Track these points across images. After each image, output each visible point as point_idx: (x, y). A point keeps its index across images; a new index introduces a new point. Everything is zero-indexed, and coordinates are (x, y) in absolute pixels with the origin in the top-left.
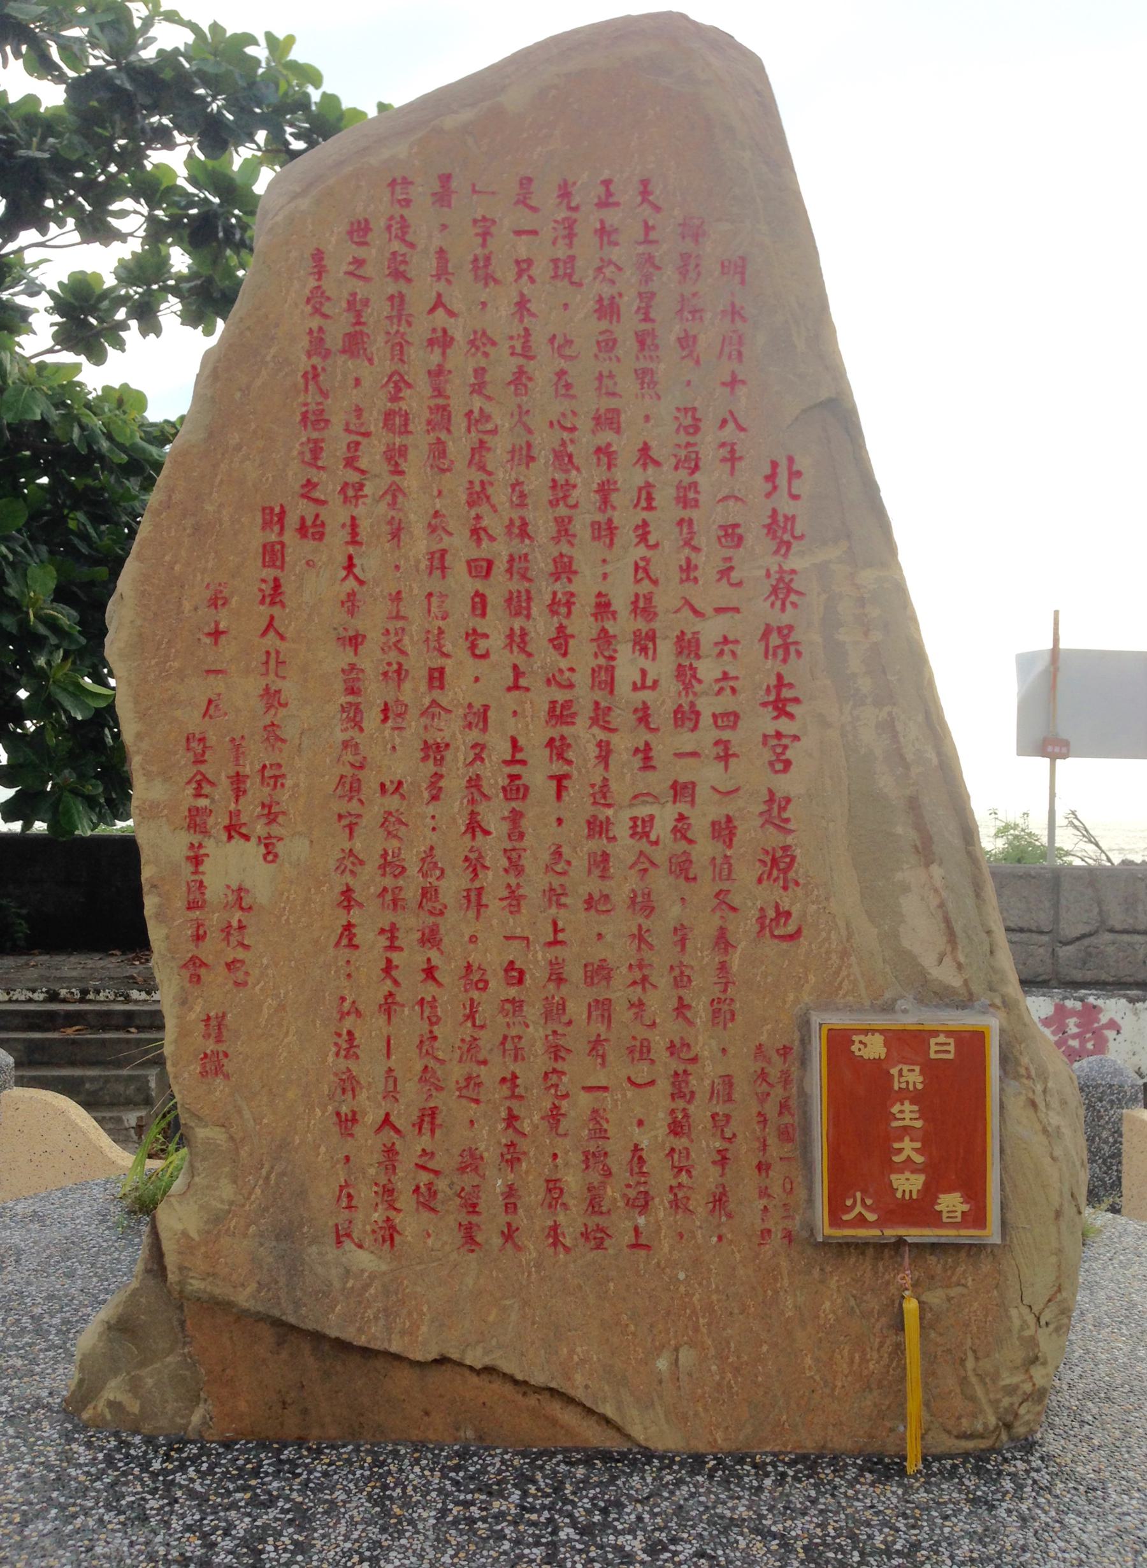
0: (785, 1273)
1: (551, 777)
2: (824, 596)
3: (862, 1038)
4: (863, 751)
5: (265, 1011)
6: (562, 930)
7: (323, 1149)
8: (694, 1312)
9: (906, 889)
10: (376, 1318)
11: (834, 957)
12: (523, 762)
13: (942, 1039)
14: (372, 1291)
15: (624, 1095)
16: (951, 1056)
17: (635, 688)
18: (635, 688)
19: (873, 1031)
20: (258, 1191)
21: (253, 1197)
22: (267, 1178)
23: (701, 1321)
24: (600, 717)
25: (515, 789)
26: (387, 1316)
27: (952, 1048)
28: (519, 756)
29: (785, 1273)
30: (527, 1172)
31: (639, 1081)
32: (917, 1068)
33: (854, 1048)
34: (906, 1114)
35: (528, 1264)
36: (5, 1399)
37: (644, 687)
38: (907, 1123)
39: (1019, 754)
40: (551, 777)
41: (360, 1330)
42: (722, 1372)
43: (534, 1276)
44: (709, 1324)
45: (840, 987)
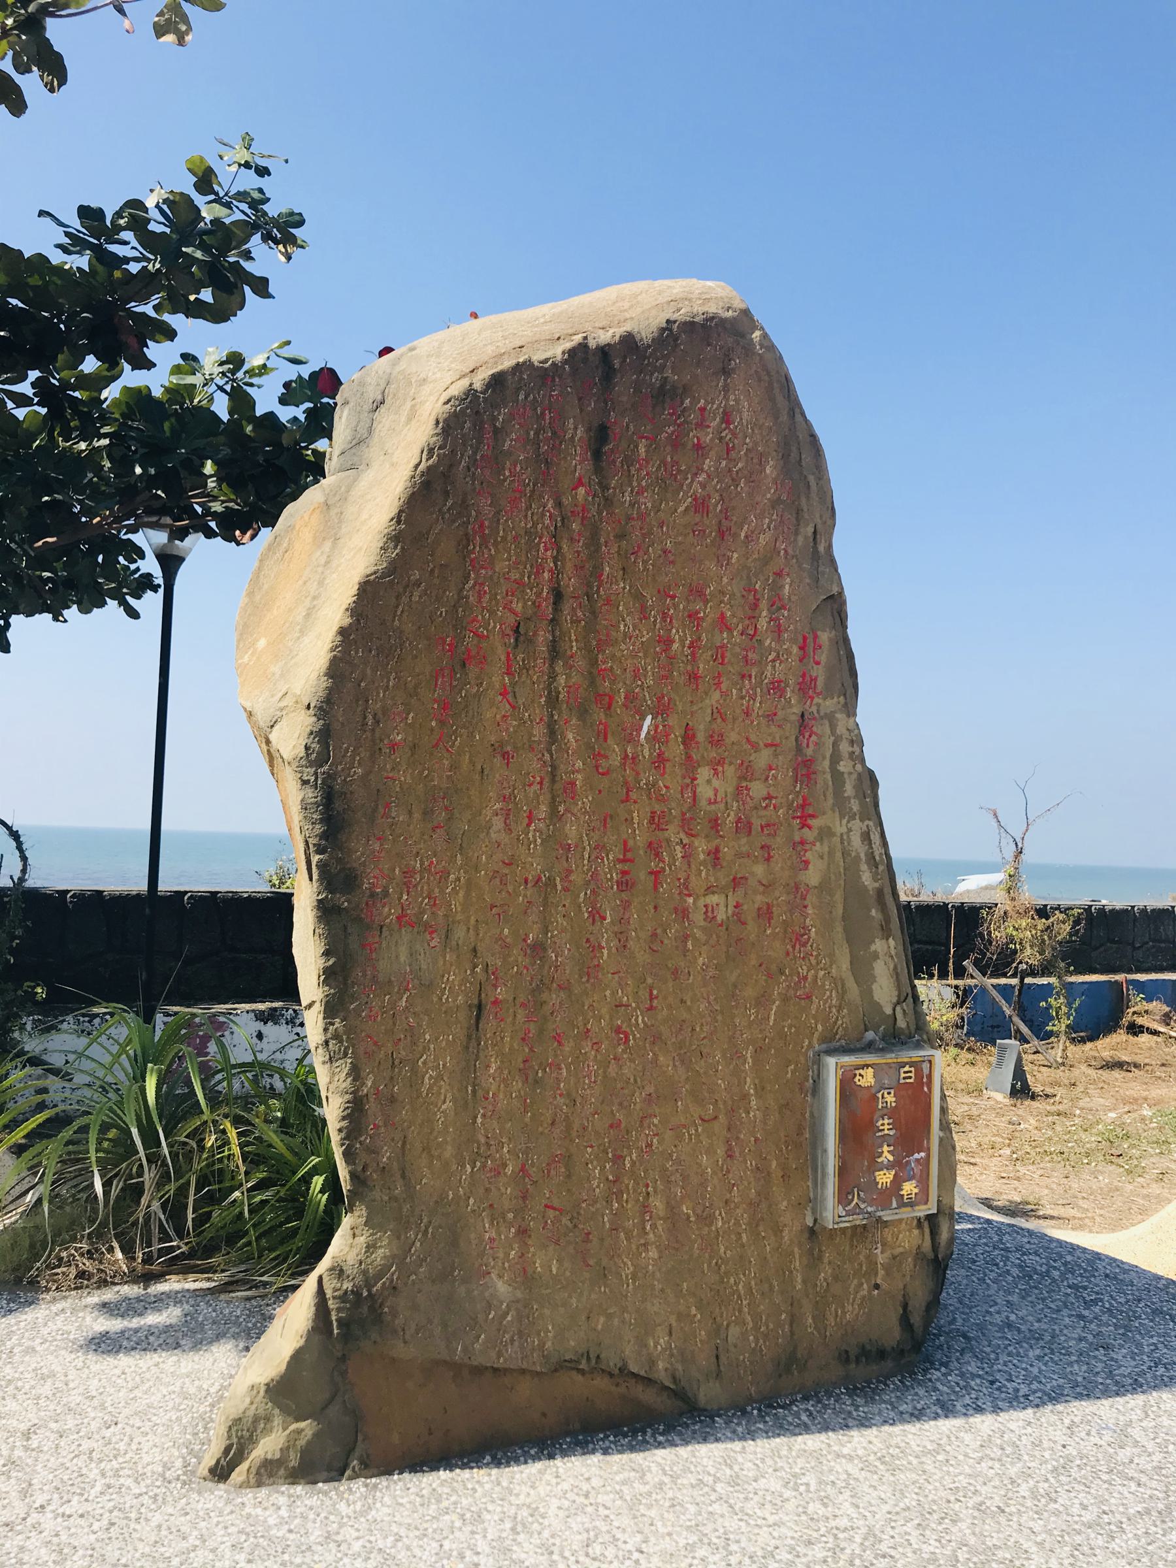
0: (797, 1256)
1: (651, 873)
2: (832, 738)
3: (861, 1071)
4: (853, 854)
5: (426, 1080)
6: (656, 997)
7: (471, 1201)
8: (739, 1297)
9: (876, 956)
10: (512, 1341)
11: (834, 1010)
12: (631, 861)
13: (907, 1068)
14: (509, 1318)
15: (697, 1130)
16: (911, 1081)
17: (710, 803)
18: (710, 803)
19: (867, 1066)
20: (418, 1244)
21: (413, 1250)
22: (426, 1231)
23: (745, 1302)
24: (686, 824)
25: (625, 884)
26: (520, 1338)
27: (912, 1075)
28: (629, 855)
29: (797, 1256)
30: (627, 1202)
31: (707, 1118)
32: (892, 1091)
33: (856, 1080)
34: (885, 1125)
35: (627, 1276)
36: (11, 1487)
37: (715, 802)
38: (886, 1132)
39: (9, 652)
40: (651, 873)
41: (499, 1355)
42: (757, 1340)
43: (631, 1287)
44: (749, 1304)
45: (837, 1033)
